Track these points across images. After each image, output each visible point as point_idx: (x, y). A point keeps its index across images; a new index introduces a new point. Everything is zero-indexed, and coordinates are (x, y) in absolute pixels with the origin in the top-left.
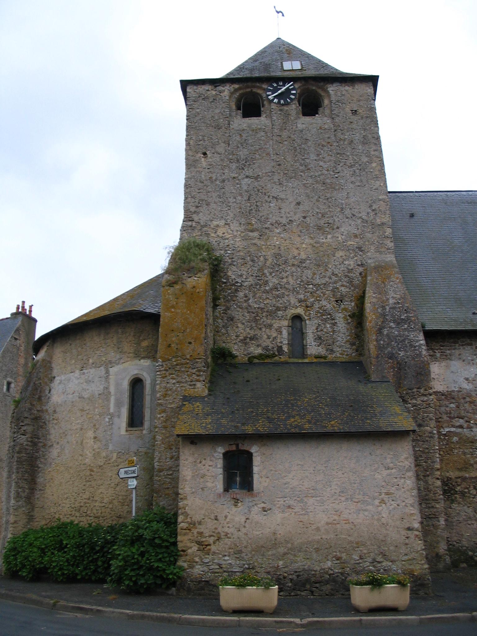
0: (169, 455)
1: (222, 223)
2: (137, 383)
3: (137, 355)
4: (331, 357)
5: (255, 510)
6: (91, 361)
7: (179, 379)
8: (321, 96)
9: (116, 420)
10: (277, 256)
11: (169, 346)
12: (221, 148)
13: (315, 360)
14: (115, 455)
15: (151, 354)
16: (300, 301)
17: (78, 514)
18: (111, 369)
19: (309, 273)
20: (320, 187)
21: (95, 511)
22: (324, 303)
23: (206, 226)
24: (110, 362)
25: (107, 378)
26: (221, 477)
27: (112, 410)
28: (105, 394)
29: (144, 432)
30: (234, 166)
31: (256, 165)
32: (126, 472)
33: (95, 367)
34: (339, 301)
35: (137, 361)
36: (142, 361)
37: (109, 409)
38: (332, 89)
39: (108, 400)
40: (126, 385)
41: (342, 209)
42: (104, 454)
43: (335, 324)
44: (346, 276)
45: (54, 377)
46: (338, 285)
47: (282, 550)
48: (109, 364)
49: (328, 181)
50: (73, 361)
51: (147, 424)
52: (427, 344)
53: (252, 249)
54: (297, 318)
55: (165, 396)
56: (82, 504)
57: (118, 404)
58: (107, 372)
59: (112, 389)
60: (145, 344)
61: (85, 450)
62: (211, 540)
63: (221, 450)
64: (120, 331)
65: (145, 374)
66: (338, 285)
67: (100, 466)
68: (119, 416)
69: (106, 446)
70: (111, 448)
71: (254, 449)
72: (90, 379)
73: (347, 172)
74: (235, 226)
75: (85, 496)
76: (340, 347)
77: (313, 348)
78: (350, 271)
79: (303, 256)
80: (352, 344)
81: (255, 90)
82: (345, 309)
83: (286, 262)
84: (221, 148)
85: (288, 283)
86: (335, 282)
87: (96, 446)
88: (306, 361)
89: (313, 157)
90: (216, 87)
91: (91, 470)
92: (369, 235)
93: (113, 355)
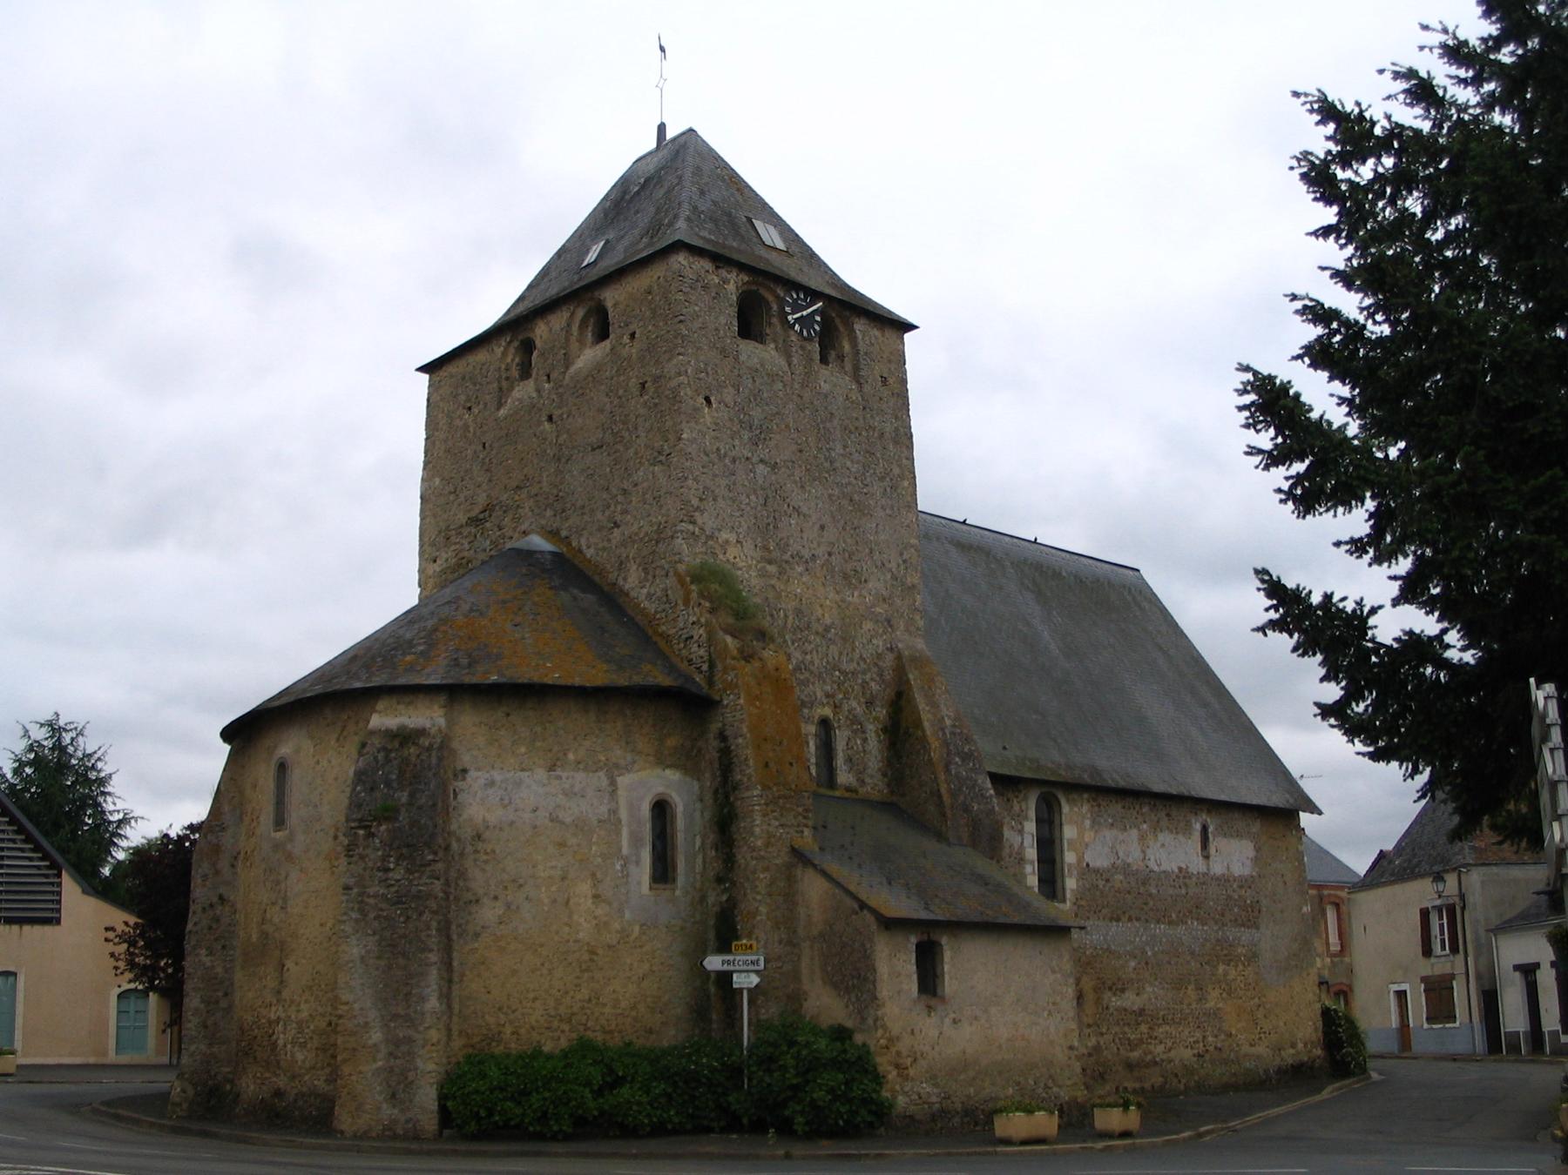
0: (776, 938)
1: (732, 538)
2: (661, 809)
3: (661, 761)
4: (862, 791)
5: (947, 1021)
6: (571, 756)
7: (783, 820)
8: (837, 329)
9: (632, 868)
10: (799, 612)
11: (767, 765)
12: (729, 394)
13: (847, 795)
14: (637, 928)
15: (687, 761)
16: (827, 696)
17: (566, 1027)
18: (619, 779)
19: (834, 650)
20: (845, 502)
21: (603, 1022)
22: (854, 704)
23: (711, 537)
24: (617, 766)
25: (613, 793)
26: (915, 977)
27: (625, 851)
28: (611, 822)
29: (678, 893)
30: (746, 435)
31: (773, 443)
32: (1528, 971)
33: (586, 769)
34: (870, 703)
35: (658, 771)
36: (668, 772)
37: (620, 850)
38: (860, 326)
39: (618, 833)
40: (646, 810)
41: (871, 551)
42: (617, 926)
43: (865, 740)
44: (876, 665)
45: (465, 771)
46: (868, 677)
47: (971, 1073)
48: (613, 771)
49: (856, 497)
50: (523, 750)
51: (681, 879)
52: (997, 793)
53: (771, 595)
54: (825, 723)
55: (768, 845)
56: (575, 1010)
57: (636, 841)
58: (613, 783)
59: (624, 814)
60: (671, 742)
61: (575, 917)
62: (909, 1061)
63: (914, 940)
64: (628, 712)
65: (674, 794)
66: (868, 677)
67: (610, 947)
68: (638, 863)
69: (621, 911)
70: (628, 915)
71: (944, 940)
72: (576, 790)
73: (877, 488)
74: (748, 545)
75: (579, 996)
76: (872, 777)
77: (844, 777)
78: (879, 656)
79: (828, 621)
80: (885, 775)
81: (762, 291)
82: (876, 719)
83: (808, 627)
84: (729, 394)
85: (812, 663)
86: (864, 673)
87: (599, 912)
88: (837, 793)
89: (839, 449)
90: (717, 267)
91: (592, 952)
92: (898, 602)
93: (618, 754)
